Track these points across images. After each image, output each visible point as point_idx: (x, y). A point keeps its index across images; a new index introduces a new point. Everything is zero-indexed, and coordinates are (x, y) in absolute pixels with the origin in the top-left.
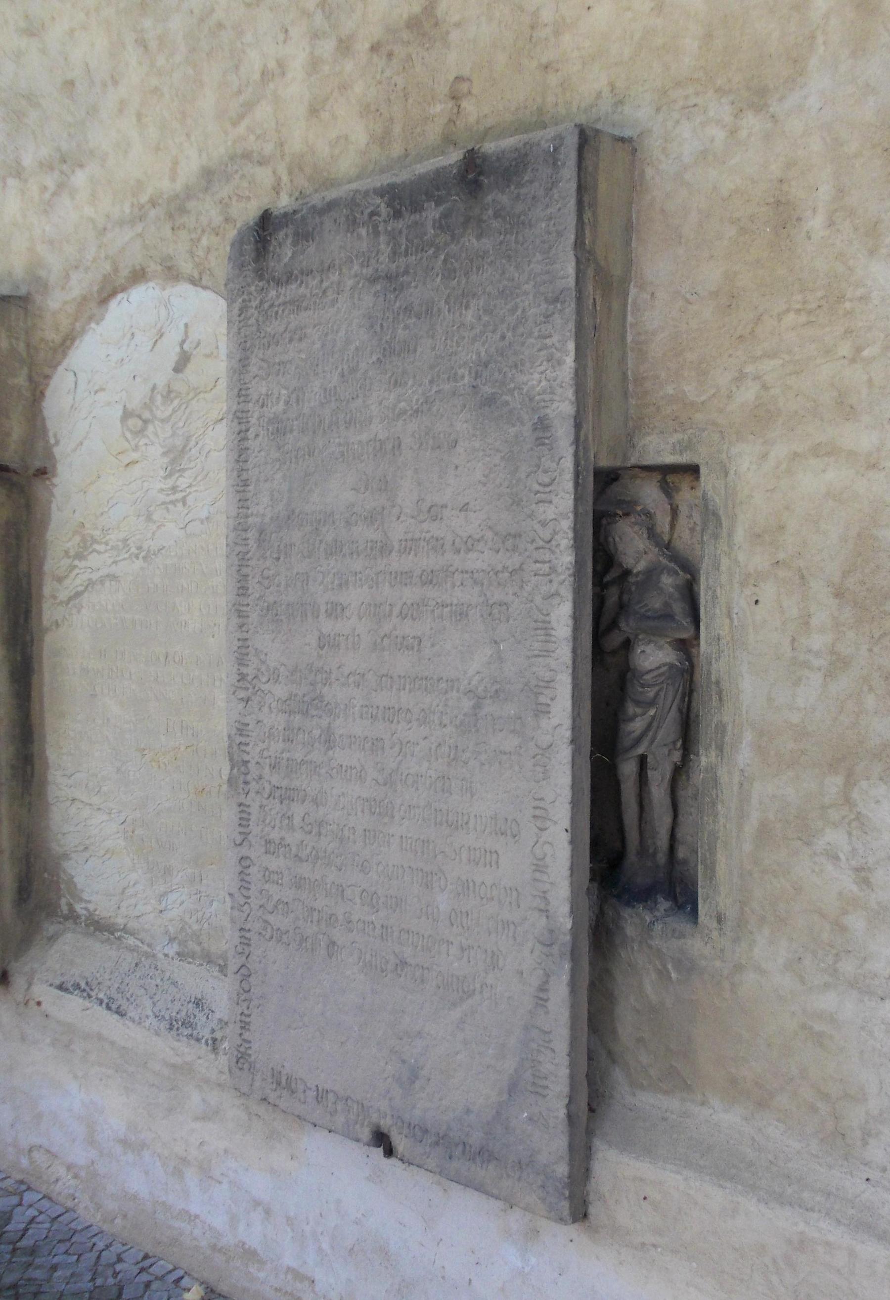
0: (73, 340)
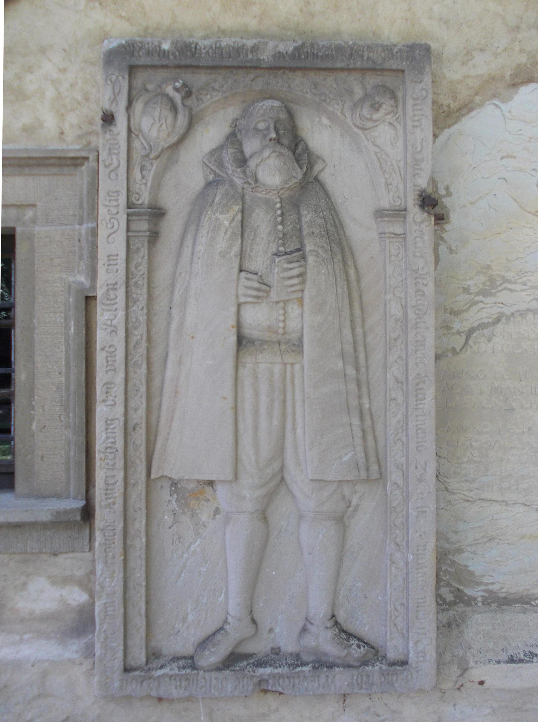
0: (471, 110)
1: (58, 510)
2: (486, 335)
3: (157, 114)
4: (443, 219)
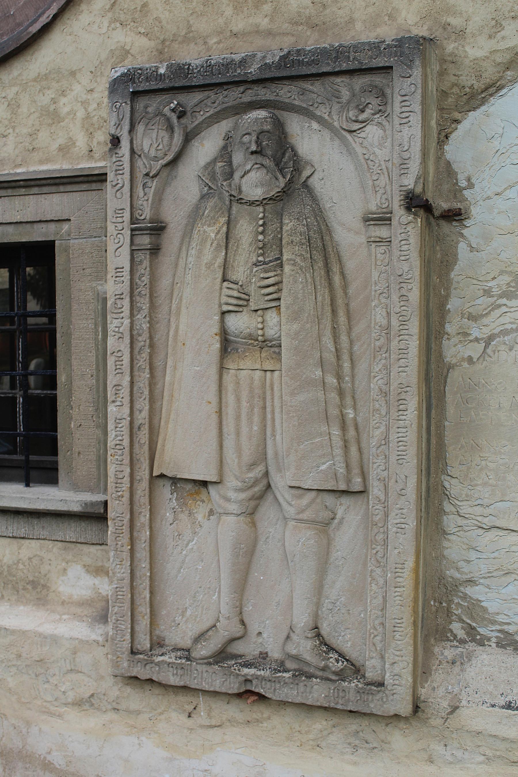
0: (501, 88)
1: (86, 502)
2: (507, 343)
3: (154, 136)
4: (460, 214)
